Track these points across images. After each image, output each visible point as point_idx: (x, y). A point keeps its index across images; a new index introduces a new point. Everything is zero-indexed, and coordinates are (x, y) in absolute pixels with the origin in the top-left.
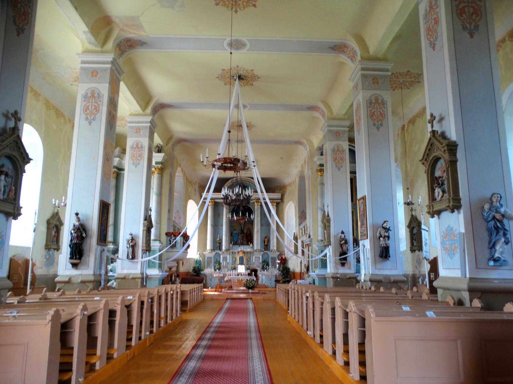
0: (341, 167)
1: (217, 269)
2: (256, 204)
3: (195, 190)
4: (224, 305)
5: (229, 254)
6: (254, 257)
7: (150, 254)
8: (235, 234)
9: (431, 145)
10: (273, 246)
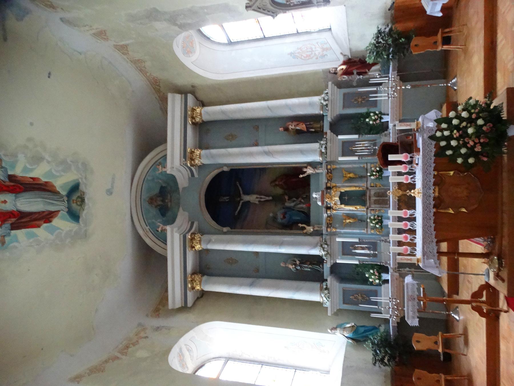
1: (380, 278)
3: (158, 329)
4: (342, 187)
5: (335, 234)
6: (341, 159)
8: (284, 217)
9: (259, 8)
10: (311, 104)
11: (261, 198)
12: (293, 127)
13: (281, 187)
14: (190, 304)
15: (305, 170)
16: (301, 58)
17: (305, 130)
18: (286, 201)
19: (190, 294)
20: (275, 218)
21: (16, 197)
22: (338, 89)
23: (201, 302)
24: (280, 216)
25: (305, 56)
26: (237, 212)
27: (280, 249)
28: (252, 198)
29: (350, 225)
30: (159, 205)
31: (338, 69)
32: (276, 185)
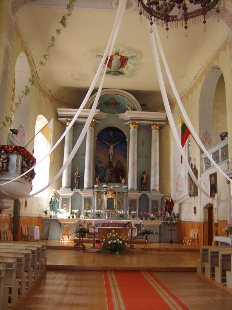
0: (205, 135)
2: (131, 126)
7: (95, 253)
8: (101, 167)
11: (111, 155)
12: (145, 176)
13: (116, 166)
14: (59, 119)
15: (124, 179)
16: (177, 181)
17: (143, 182)
18: (109, 169)
19: (64, 119)
20: (100, 162)
21: (118, 60)
22: (160, 198)
23: (59, 124)
24: (101, 165)
25: (179, 183)
26: (104, 141)
27: (87, 168)
28: (111, 151)
29: (98, 202)
30: (110, 102)
31: (170, 198)
32: (118, 163)
